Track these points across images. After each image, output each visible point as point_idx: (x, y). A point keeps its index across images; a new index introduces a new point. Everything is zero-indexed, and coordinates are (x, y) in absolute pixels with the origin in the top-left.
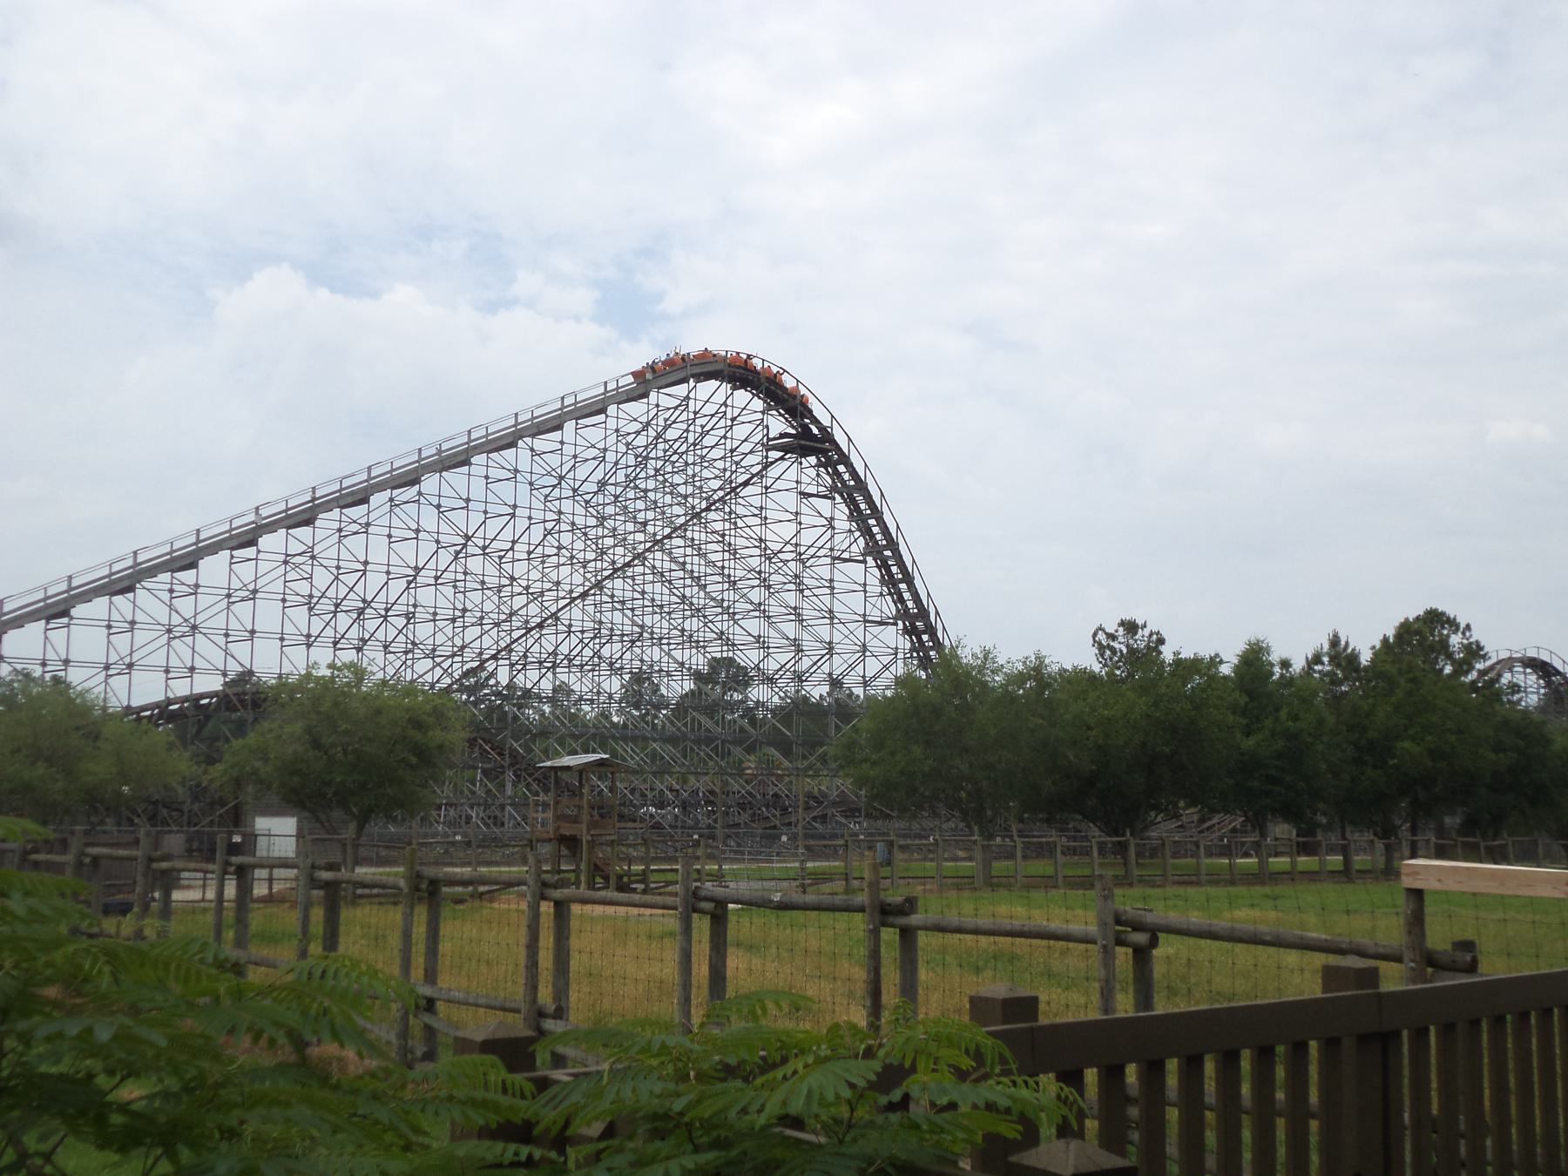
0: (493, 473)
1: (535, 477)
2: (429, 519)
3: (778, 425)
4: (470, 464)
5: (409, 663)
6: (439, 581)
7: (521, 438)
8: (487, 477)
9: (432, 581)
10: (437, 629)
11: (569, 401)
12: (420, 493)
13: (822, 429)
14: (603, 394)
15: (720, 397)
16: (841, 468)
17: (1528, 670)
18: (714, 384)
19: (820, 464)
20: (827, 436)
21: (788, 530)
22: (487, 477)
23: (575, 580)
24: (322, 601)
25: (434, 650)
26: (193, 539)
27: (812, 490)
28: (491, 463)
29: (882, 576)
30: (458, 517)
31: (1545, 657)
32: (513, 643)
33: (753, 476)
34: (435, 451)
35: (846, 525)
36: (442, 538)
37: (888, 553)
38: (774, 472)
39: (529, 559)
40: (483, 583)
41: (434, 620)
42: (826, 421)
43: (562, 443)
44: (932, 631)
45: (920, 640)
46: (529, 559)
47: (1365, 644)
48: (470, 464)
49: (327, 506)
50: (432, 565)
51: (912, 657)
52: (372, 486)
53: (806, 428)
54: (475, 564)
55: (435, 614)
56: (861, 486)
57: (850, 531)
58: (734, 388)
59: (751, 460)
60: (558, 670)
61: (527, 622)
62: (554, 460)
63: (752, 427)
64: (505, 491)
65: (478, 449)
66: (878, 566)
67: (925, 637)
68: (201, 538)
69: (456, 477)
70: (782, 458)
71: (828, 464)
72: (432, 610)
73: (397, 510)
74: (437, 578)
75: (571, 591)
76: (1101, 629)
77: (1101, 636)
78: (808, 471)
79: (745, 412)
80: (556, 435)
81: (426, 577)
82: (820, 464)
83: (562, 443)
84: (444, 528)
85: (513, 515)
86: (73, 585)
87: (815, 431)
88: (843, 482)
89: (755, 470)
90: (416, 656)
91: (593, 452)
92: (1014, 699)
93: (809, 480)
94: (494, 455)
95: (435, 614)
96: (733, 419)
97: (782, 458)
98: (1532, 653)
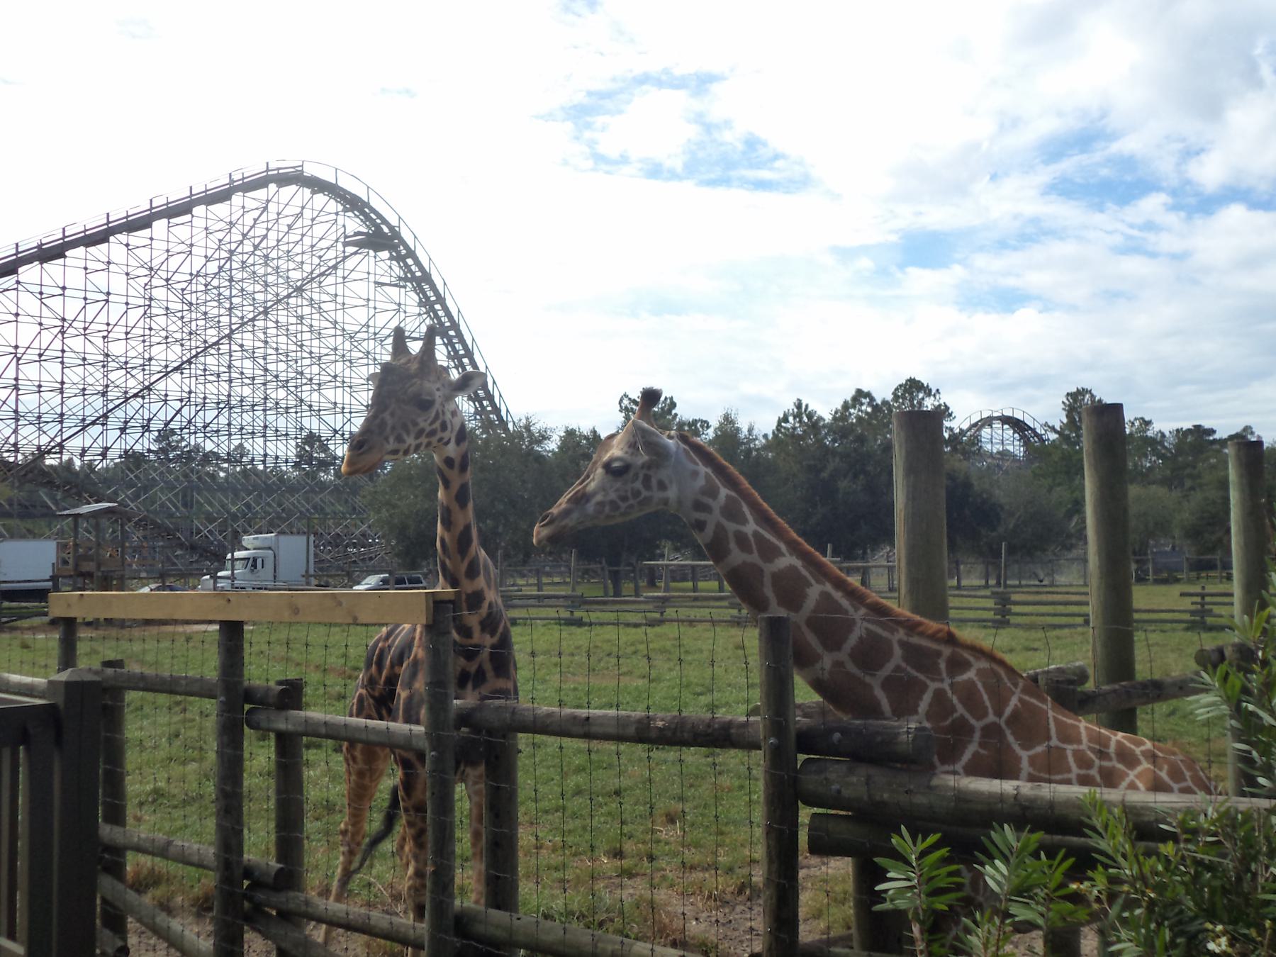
0: (91, 265)
1: (130, 269)
2: (29, 304)
3: (354, 224)
4: (65, 257)
5: (146, 406)
6: (43, 358)
7: (113, 234)
8: (86, 268)
9: (124, 336)
10: (42, 401)
11: (236, 177)
12: (18, 282)
13: (391, 228)
14: (107, 224)
15: (297, 201)
16: (410, 261)
17: (1006, 426)
18: (293, 188)
19: (391, 258)
20: (395, 234)
21: (361, 315)
22: (86, 268)
23: (175, 354)
24: (29, 351)
25: (39, 417)
26: (14, 251)
27: (386, 280)
28: (89, 257)
29: (449, 352)
30: (56, 303)
31: (1019, 416)
32: (108, 412)
33: (330, 268)
34: (35, 245)
35: (417, 310)
36: (44, 321)
37: (452, 333)
38: (350, 264)
39: (127, 339)
40: (84, 359)
41: (39, 392)
42: (393, 221)
43: (151, 239)
44: (490, 397)
45: (481, 405)
46: (127, 339)
47: (825, 410)
48: (65, 257)
49: (74, 244)
50: (123, 322)
51: (475, 419)
52: (65, 243)
53: (378, 227)
54: (76, 343)
55: (40, 386)
56: (427, 277)
57: (420, 315)
58: (314, 193)
59: (331, 254)
60: (268, 412)
61: (126, 392)
62: (144, 254)
63: (328, 225)
64: (100, 279)
65: (199, 202)
66: (444, 344)
67: (485, 403)
68: (20, 250)
69: (53, 267)
70: (355, 253)
71: (400, 258)
72: (37, 383)
73: (210, 236)
74: (40, 355)
75: (166, 366)
76: (626, 396)
77: (626, 402)
78: (381, 264)
79: (322, 213)
80: (146, 233)
81: (119, 332)
82: (391, 258)
83: (151, 239)
84: (46, 312)
85: (107, 301)
86: (20, 250)
87: (386, 230)
88: (413, 273)
89: (331, 263)
90: (327, 370)
91: (183, 248)
92: (792, 435)
93: (382, 272)
94: (91, 249)
95: (40, 386)
96: (313, 220)
97: (355, 253)
98: (1008, 413)
